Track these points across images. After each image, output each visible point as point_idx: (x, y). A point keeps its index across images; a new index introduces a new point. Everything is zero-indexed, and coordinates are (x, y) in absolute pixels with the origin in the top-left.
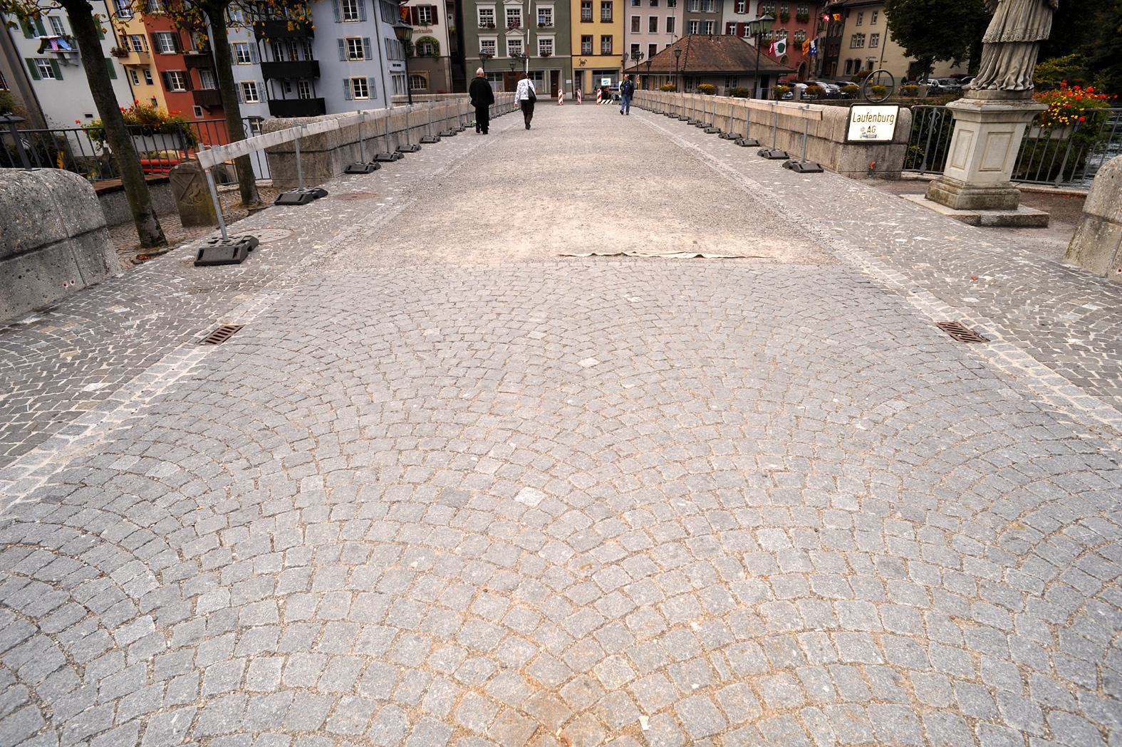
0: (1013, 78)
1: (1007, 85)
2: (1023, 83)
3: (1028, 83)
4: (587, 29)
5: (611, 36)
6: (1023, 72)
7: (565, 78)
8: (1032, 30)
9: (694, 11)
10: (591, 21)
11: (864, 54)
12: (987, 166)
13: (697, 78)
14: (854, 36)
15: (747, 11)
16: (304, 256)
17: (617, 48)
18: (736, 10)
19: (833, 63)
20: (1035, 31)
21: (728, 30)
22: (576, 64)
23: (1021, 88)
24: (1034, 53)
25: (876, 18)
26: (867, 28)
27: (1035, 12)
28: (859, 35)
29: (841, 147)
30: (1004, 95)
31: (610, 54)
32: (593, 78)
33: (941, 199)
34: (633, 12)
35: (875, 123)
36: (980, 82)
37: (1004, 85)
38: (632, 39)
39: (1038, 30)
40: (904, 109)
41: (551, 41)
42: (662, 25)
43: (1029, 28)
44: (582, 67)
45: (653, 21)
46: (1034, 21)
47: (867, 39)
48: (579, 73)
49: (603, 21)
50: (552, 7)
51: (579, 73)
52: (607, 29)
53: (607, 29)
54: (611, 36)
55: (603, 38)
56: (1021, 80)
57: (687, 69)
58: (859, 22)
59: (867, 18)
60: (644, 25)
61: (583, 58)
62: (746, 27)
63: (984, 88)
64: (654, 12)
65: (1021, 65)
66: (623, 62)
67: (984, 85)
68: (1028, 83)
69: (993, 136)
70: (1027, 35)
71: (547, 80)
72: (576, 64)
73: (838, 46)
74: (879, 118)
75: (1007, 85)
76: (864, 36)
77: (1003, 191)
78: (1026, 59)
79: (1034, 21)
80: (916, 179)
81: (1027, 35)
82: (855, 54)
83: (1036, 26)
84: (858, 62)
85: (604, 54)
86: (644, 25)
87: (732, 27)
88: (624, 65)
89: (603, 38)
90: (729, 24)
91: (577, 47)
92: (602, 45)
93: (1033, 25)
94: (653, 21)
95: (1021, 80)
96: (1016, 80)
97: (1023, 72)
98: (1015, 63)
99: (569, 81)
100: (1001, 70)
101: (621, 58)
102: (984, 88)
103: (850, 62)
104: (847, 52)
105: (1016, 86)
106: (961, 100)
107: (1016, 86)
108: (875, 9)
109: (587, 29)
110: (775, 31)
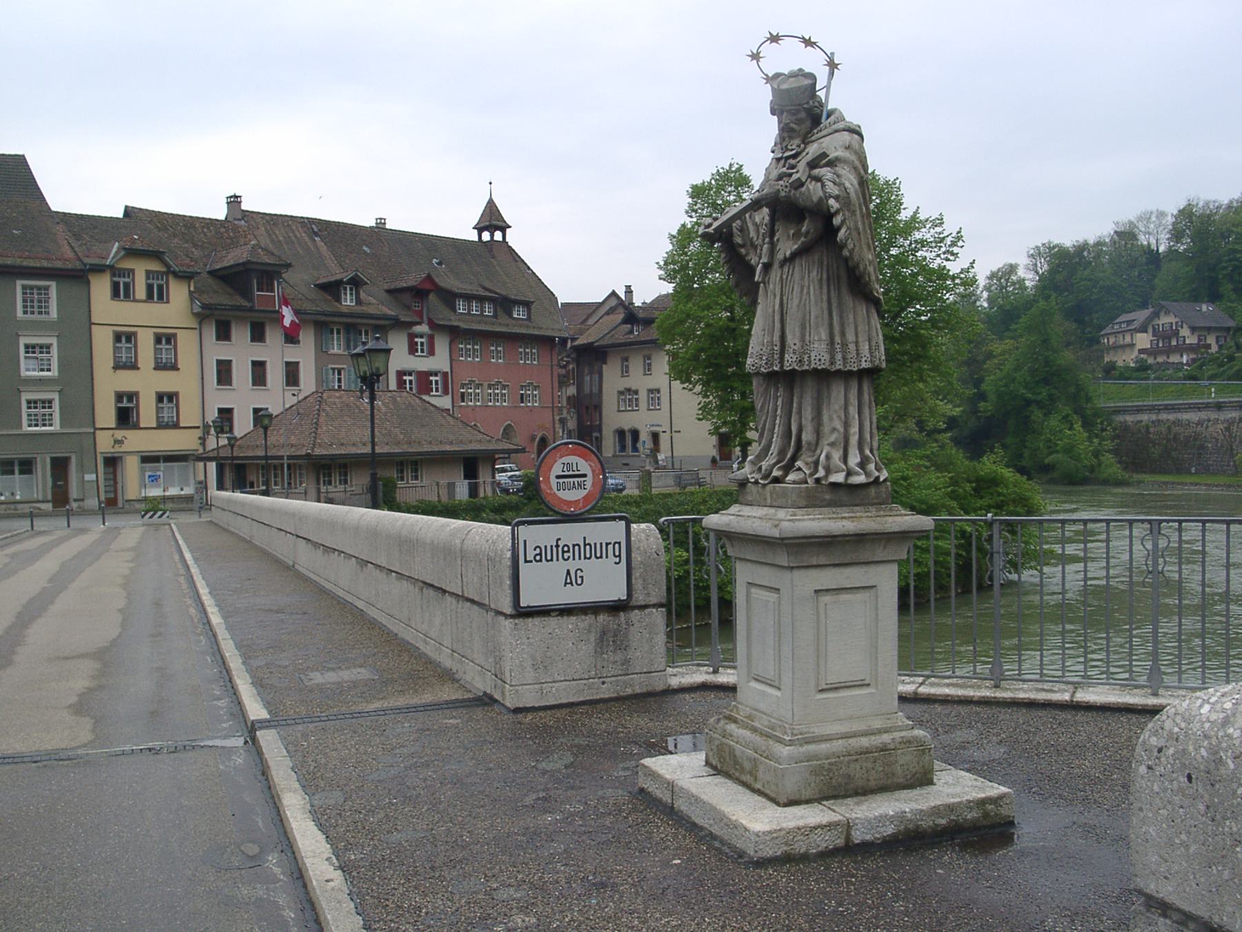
0: (837, 455)
1: (828, 471)
2: (863, 465)
3: (872, 466)
4: (127, 381)
5: (176, 394)
6: (854, 440)
7: (82, 469)
8: (844, 345)
9: (336, 351)
10: (134, 366)
11: (642, 420)
12: (833, 679)
13: (340, 466)
14: (621, 393)
15: (432, 352)
16: (725, 552)
17: (189, 414)
18: (413, 349)
19: (595, 434)
20: (852, 347)
21: (401, 384)
22: (105, 443)
23: (860, 479)
24: (866, 396)
25: (650, 364)
26: (638, 380)
27: (840, 304)
28: (629, 390)
29: (508, 623)
30: (827, 497)
31: (176, 426)
32: (143, 471)
33: (742, 770)
34: (217, 351)
35: (582, 563)
36: (765, 465)
37: (821, 473)
38: (219, 399)
39: (857, 343)
40: (643, 526)
41: (50, 402)
42: (275, 375)
43: (838, 339)
44: (117, 449)
45: (259, 369)
46: (842, 325)
47: (643, 396)
48: (112, 462)
49: (160, 366)
50: (54, 341)
51: (112, 462)
52: (167, 382)
53: (167, 382)
54: (176, 394)
55: (160, 397)
56: (854, 459)
57: (318, 451)
58: (625, 372)
59: (636, 364)
60: (242, 373)
61: (120, 434)
62: (433, 378)
63: (777, 480)
64: (259, 352)
65: (847, 425)
66: (203, 440)
67: (776, 473)
68: (872, 466)
69: (827, 599)
70: (839, 356)
71: (44, 476)
72: (105, 443)
73: (598, 407)
74: (590, 551)
75: (828, 471)
76: (636, 392)
77: (886, 738)
78: (853, 411)
79: (842, 325)
80: (704, 687)
81: (839, 356)
82: (628, 421)
83: (850, 337)
84: (635, 434)
85: (161, 426)
86: (242, 373)
87: (407, 378)
88: (203, 444)
89: (160, 397)
90: (401, 374)
91: (106, 414)
92: (159, 410)
93: (843, 334)
94: (259, 369)
95: (854, 459)
96: (845, 459)
97: (854, 440)
98: (832, 421)
99: (90, 477)
100: (807, 436)
101: (199, 433)
102: (777, 480)
103: (621, 433)
104: (614, 418)
105: (849, 473)
106: (734, 509)
107: (849, 473)
108: (646, 352)
109: (127, 381)
110: (486, 384)
